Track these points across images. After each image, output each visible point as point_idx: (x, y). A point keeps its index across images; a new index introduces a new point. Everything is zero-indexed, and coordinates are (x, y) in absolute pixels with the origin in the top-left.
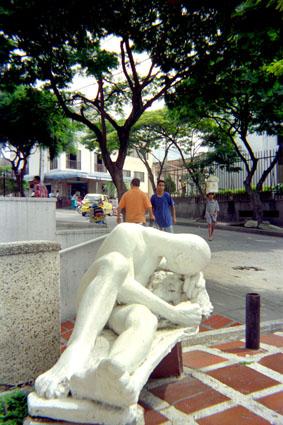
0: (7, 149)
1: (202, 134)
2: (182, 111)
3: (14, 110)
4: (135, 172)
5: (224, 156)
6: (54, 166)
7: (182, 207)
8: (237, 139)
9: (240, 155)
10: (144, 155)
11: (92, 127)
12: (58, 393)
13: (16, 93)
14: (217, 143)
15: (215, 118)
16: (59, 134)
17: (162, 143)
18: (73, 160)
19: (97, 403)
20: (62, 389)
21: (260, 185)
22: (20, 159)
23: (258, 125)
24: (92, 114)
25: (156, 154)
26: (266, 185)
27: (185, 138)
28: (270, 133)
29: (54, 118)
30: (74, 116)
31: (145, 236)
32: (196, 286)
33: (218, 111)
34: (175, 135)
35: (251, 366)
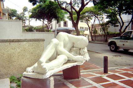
0: (45, 21)
1: (107, 15)
2: (99, 6)
3: (46, 8)
4: (85, 28)
5: (113, 21)
6: (60, 26)
7: (99, 38)
8: (118, 17)
9: (119, 21)
10: (87, 22)
11: (69, 12)
12: (30, 71)
13: (46, 3)
14: (111, 18)
15: (110, 9)
16: (59, 15)
17: (93, 18)
18: (65, 23)
19: (38, 73)
20: (32, 70)
21: (124, 31)
22: (49, 24)
23: (126, 11)
24: (69, 8)
25: (91, 22)
26: (127, 31)
27: (101, 16)
28: (129, 14)
29: (58, 10)
30: (63, 9)
31: (68, 36)
32: (84, 52)
33: (112, 6)
34: (97, 15)
35: (103, 77)
